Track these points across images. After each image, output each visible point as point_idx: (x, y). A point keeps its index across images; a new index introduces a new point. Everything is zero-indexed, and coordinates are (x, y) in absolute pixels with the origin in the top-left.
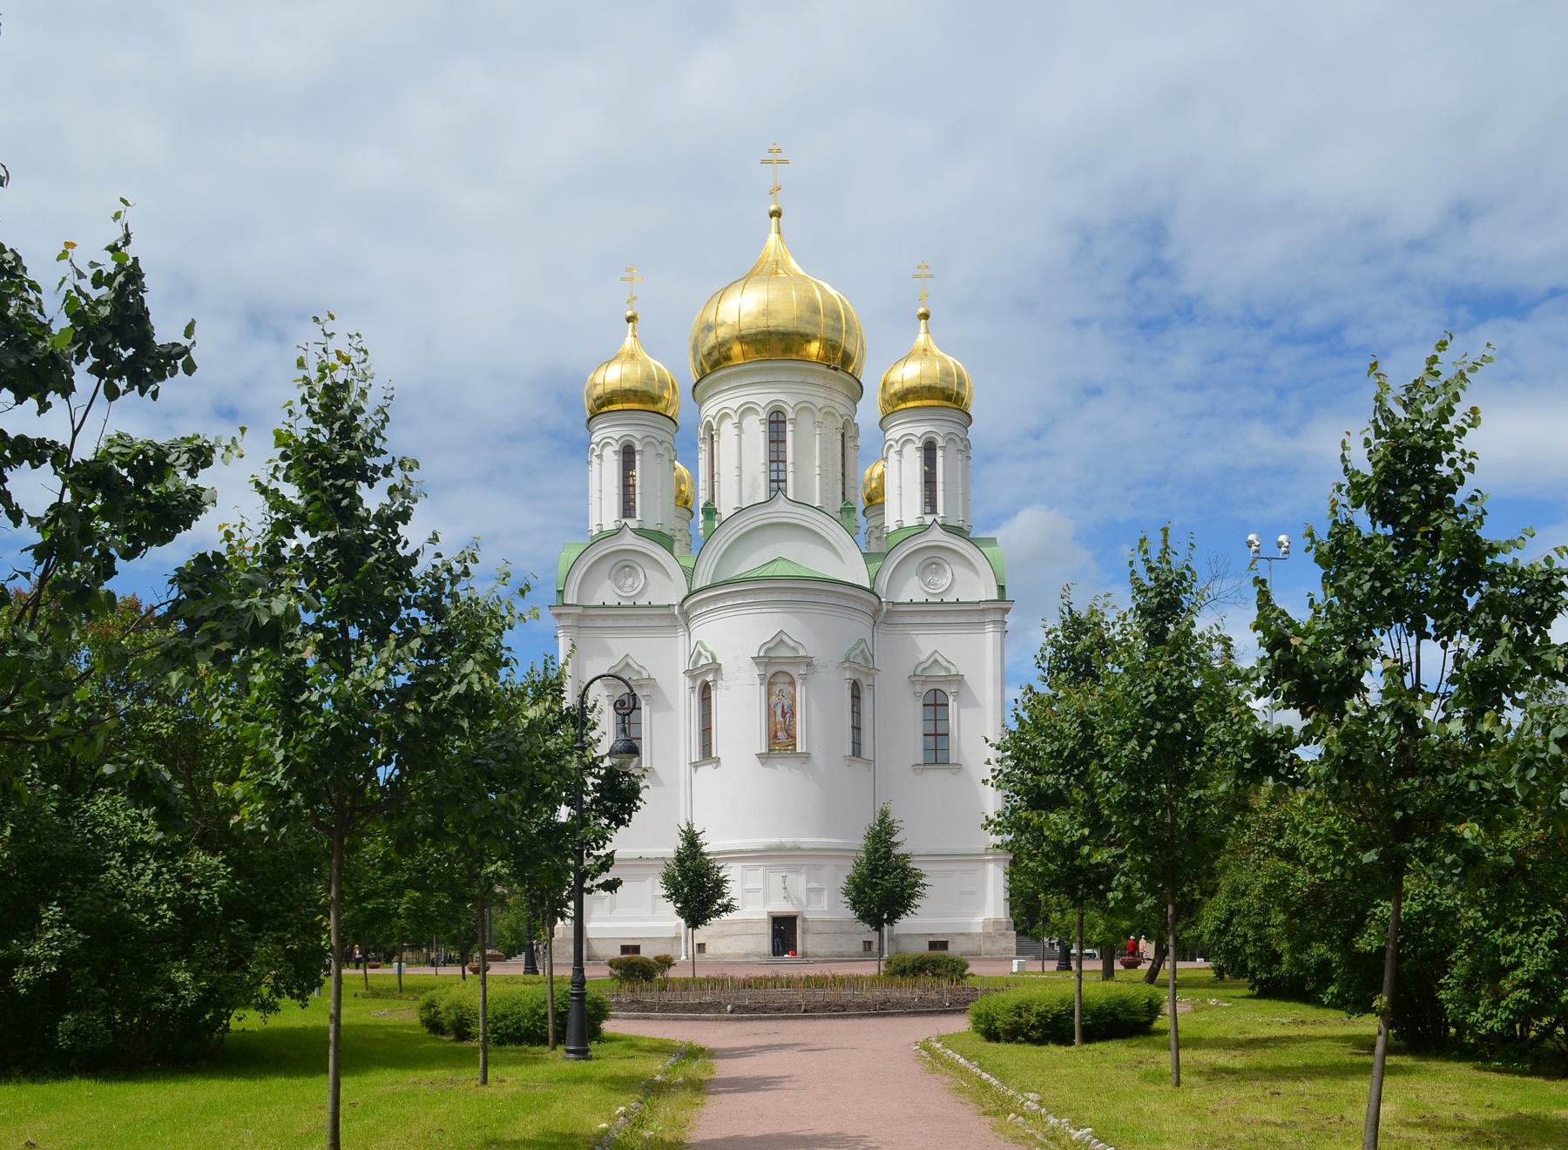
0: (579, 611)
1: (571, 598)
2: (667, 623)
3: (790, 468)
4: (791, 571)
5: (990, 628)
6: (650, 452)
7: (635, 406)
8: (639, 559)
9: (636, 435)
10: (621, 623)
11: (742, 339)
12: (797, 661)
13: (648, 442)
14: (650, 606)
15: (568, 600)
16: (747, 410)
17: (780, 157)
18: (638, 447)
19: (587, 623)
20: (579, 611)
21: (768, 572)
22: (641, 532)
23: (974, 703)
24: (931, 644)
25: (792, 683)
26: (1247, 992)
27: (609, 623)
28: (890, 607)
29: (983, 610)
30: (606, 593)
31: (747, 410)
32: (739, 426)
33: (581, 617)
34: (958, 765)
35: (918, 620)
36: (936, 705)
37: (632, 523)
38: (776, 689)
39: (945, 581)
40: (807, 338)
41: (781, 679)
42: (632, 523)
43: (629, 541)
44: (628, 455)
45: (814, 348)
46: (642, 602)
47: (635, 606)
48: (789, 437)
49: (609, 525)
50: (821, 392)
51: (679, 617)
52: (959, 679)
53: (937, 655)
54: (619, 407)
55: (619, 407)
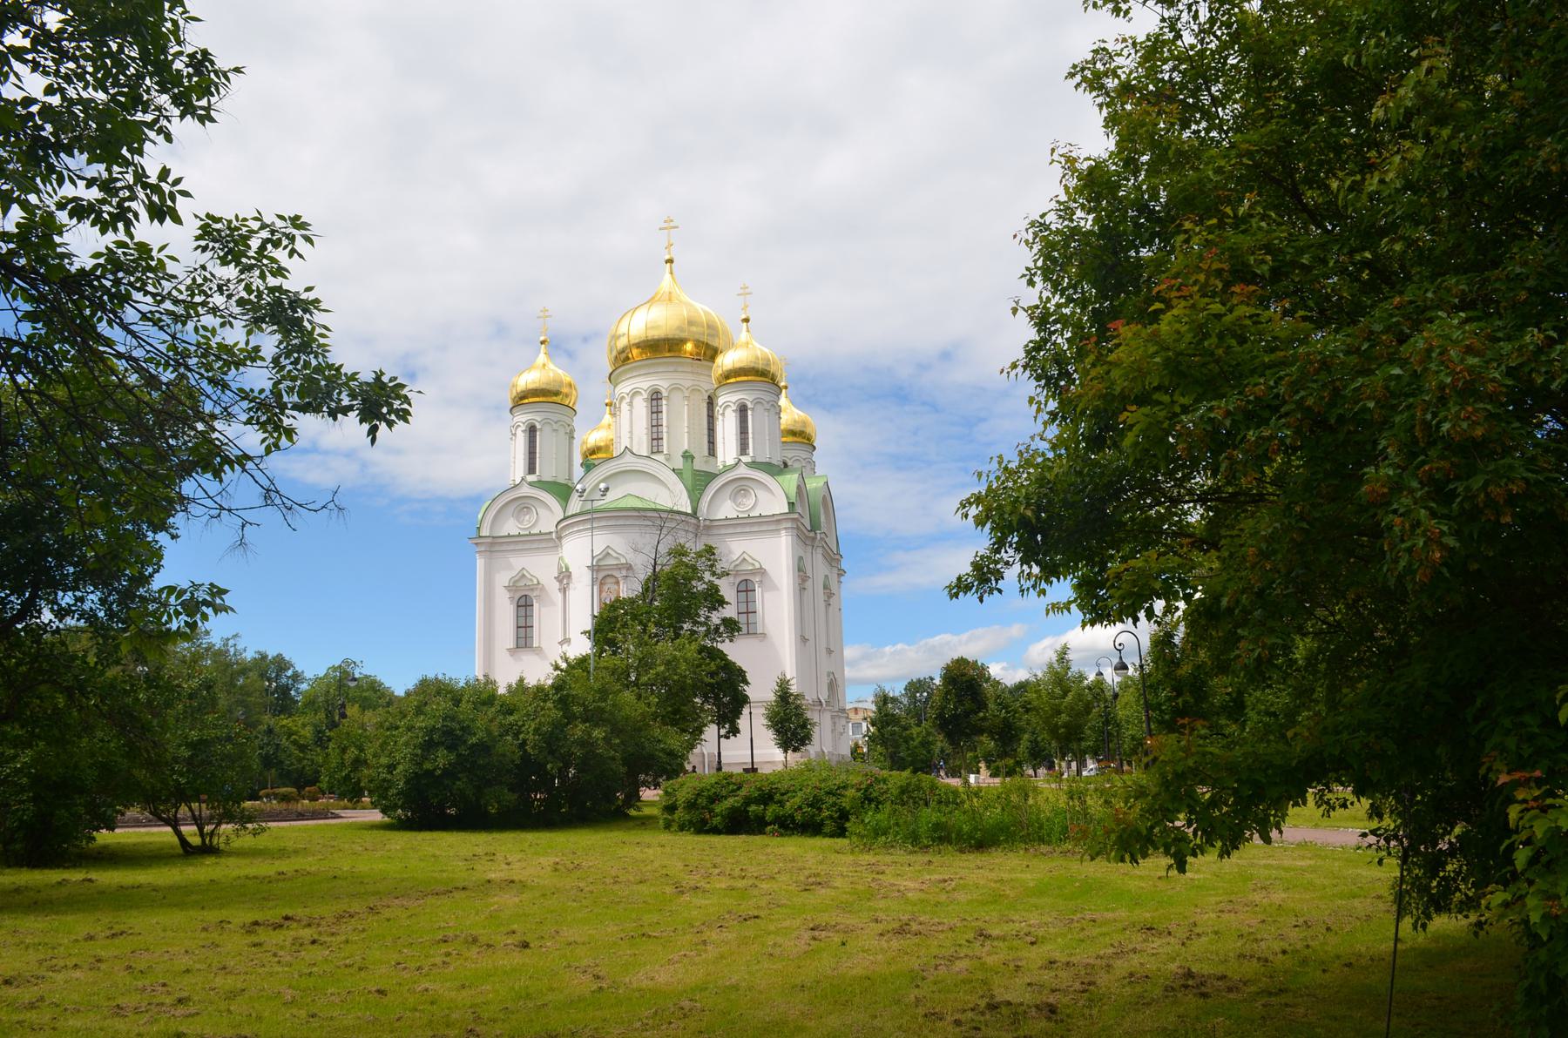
0: (489, 540)
1: (485, 532)
2: (551, 544)
3: (665, 429)
4: (639, 505)
5: (783, 533)
6: (547, 429)
7: (745, 378)
8: (530, 501)
9: (536, 418)
10: (535, 546)
11: (638, 345)
12: (619, 567)
13: (546, 422)
14: (541, 534)
15: (483, 534)
16: (635, 393)
17: (672, 224)
18: (538, 426)
19: (497, 548)
20: (489, 540)
21: (622, 504)
22: (754, 465)
23: (774, 588)
24: (520, 562)
25: (618, 583)
26: (376, 816)
27: (512, 547)
28: (707, 523)
29: (778, 521)
30: (510, 527)
31: (635, 393)
32: (631, 404)
33: (492, 544)
34: (539, 649)
35: (731, 531)
36: (524, 606)
37: (531, 478)
38: (606, 588)
39: (751, 502)
40: (683, 341)
41: (610, 580)
42: (745, 459)
43: (743, 471)
44: (743, 410)
45: (689, 347)
46: (755, 513)
47: (530, 535)
48: (664, 409)
49: (730, 461)
50: (690, 376)
51: (551, 541)
52: (761, 572)
53: (745, 556)
54: (531, 400)
55: (531, 400)
